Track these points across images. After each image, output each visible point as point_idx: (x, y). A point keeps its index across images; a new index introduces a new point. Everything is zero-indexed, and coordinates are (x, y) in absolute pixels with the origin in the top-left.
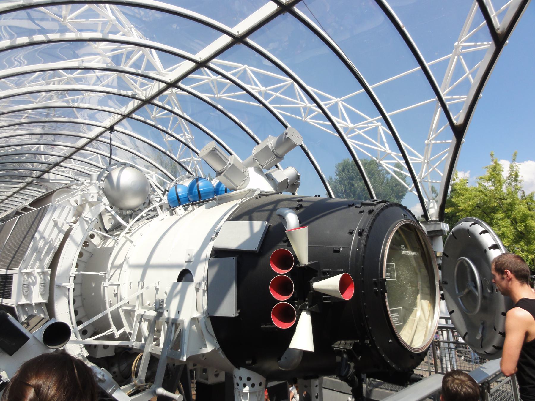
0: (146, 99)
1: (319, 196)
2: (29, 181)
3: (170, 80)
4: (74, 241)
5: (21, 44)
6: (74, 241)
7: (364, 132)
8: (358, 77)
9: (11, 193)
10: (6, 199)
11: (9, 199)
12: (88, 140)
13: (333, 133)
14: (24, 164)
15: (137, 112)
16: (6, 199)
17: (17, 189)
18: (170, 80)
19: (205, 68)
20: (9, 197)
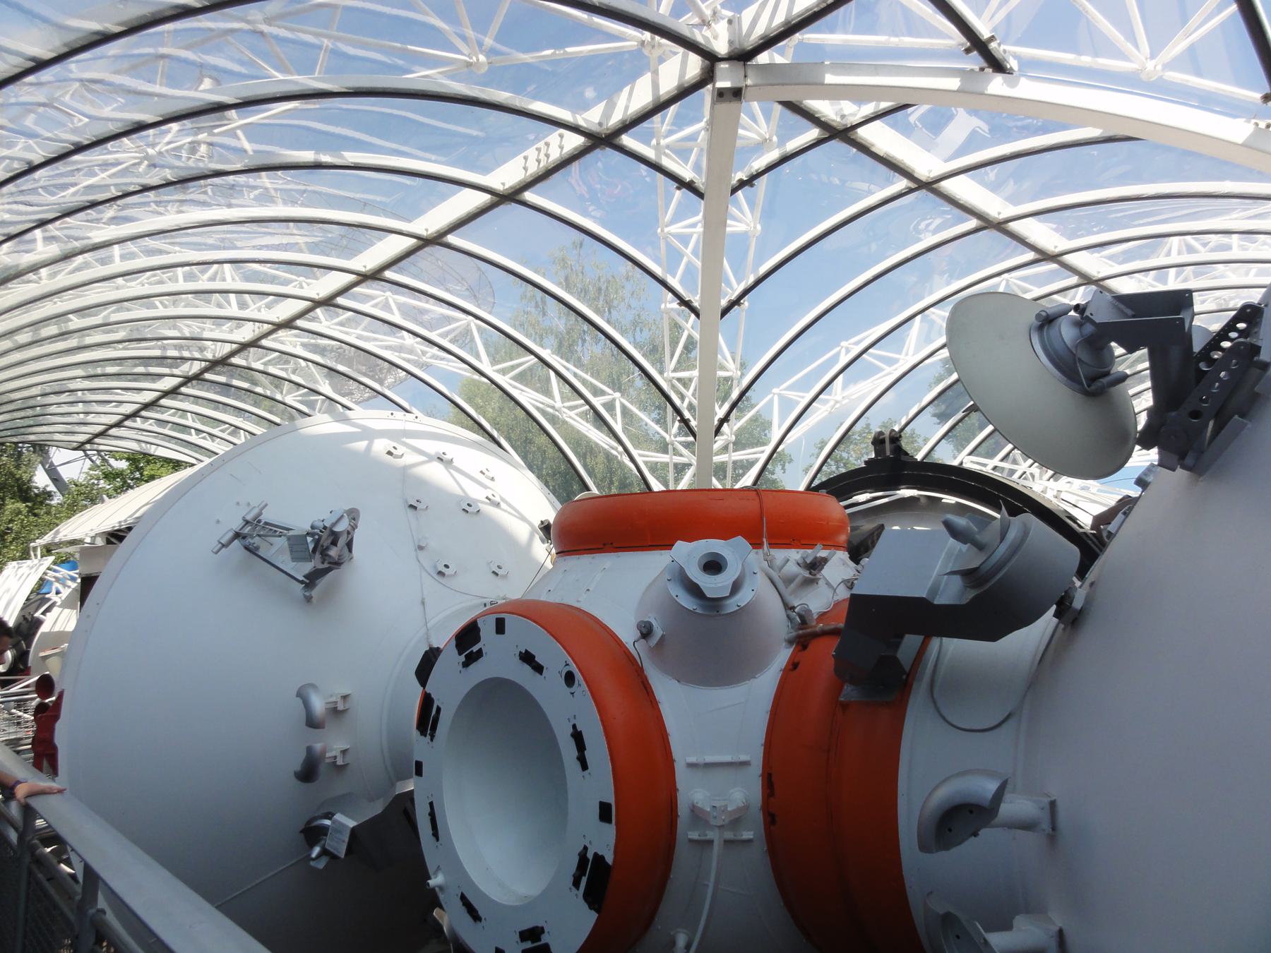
0: (504, 190)
1: (570, 889)
2: (190, 374)
3: (503, 184)
4: (655, 85)
5: (390, 167)
6: (655, 85)
7: (883, 370)
8: (642, 158)
9: (119, 417)
10: (118, 425)
11: (127, 423)
12: (411, 242)
13: (404, 46)
14: (41, 418)
15: (539, 186)
16: (118, 425)
17: (86, 437)
18: (503, 184)
19: (126, 29)
20: (128, 417)
